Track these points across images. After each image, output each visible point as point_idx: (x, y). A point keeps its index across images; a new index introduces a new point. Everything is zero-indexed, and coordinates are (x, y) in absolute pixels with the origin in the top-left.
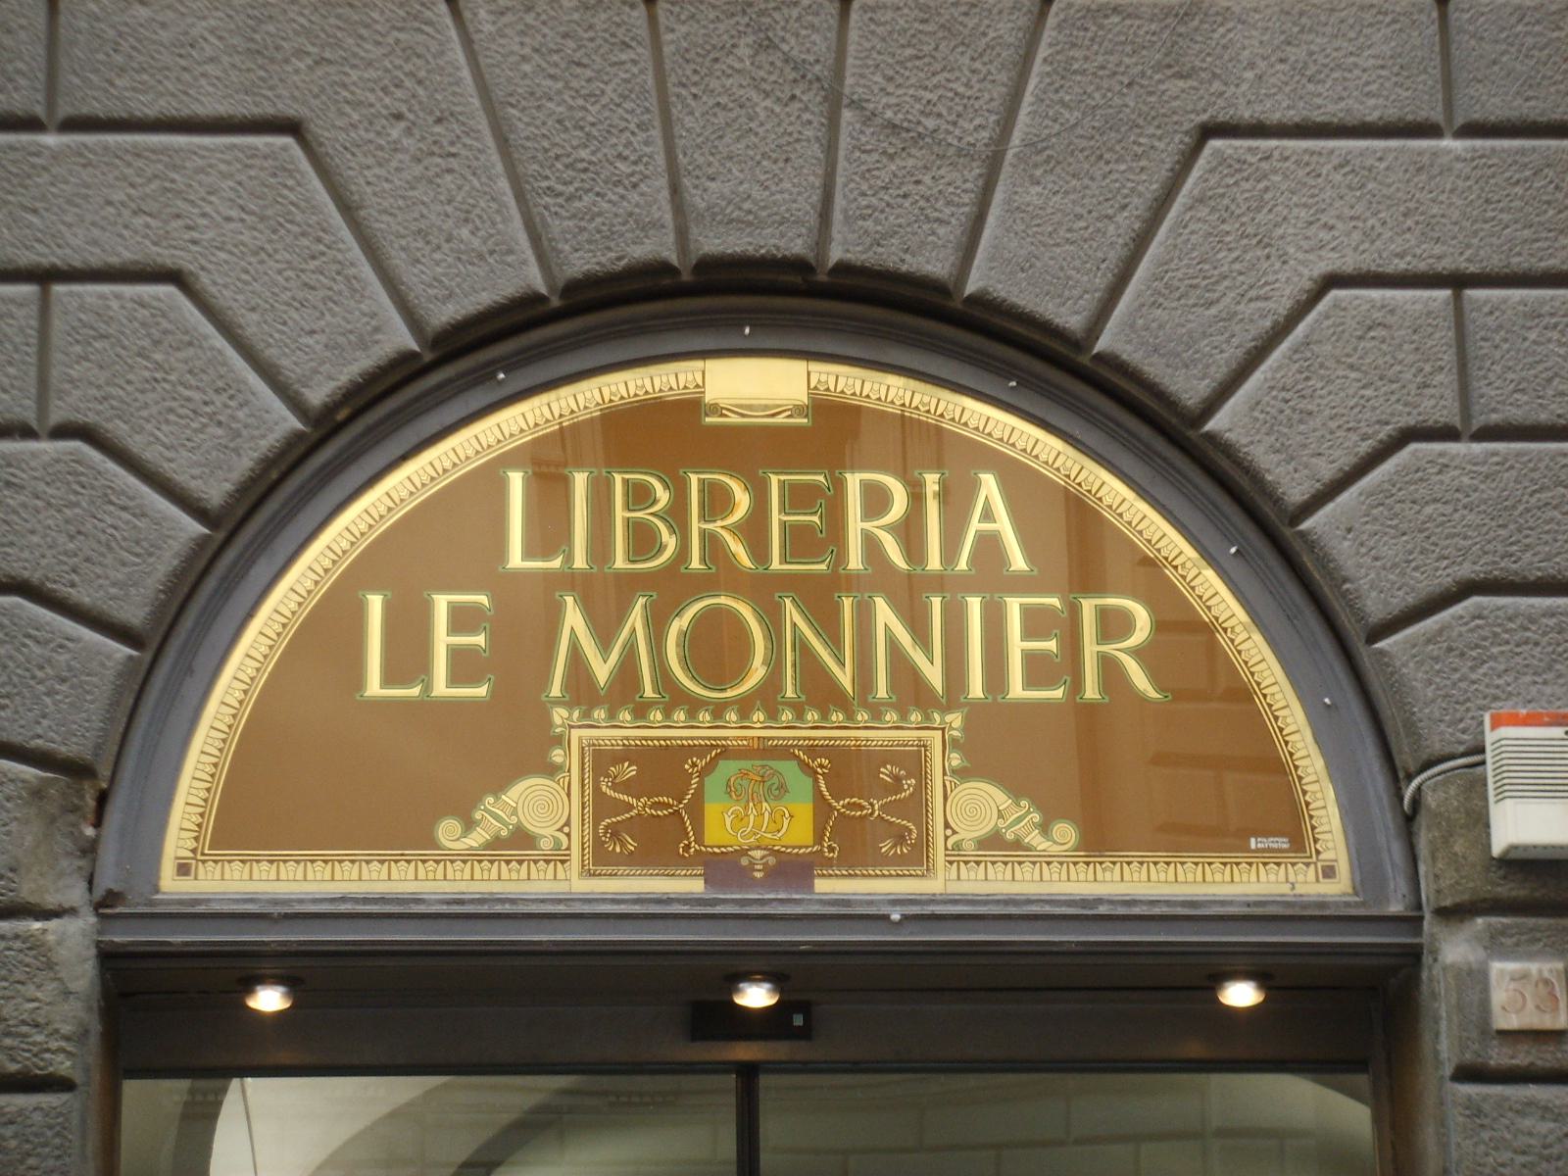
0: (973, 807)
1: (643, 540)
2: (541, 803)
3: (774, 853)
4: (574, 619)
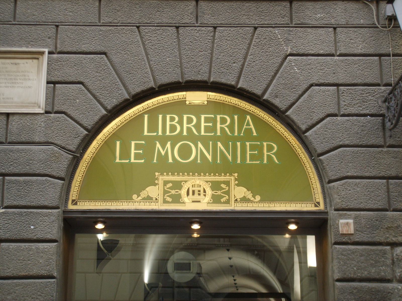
0: (240, 192)
1: (173, 128)
4: (158, 145)
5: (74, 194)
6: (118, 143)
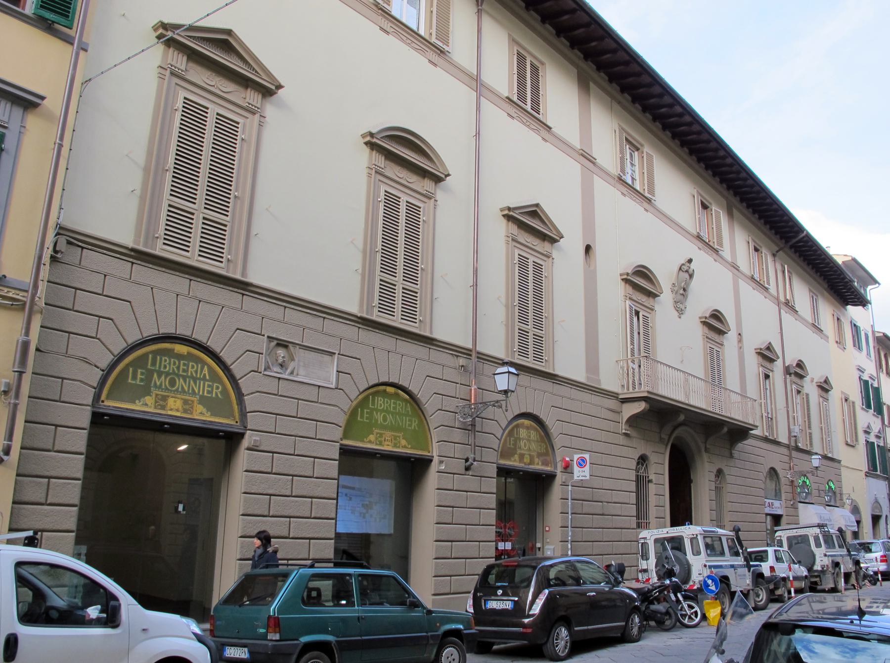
0: (200, 408)
2: (149, 400)
3: (479, 12)
4: (155, 375)
5: (103, 397)
6: (131, 369)
